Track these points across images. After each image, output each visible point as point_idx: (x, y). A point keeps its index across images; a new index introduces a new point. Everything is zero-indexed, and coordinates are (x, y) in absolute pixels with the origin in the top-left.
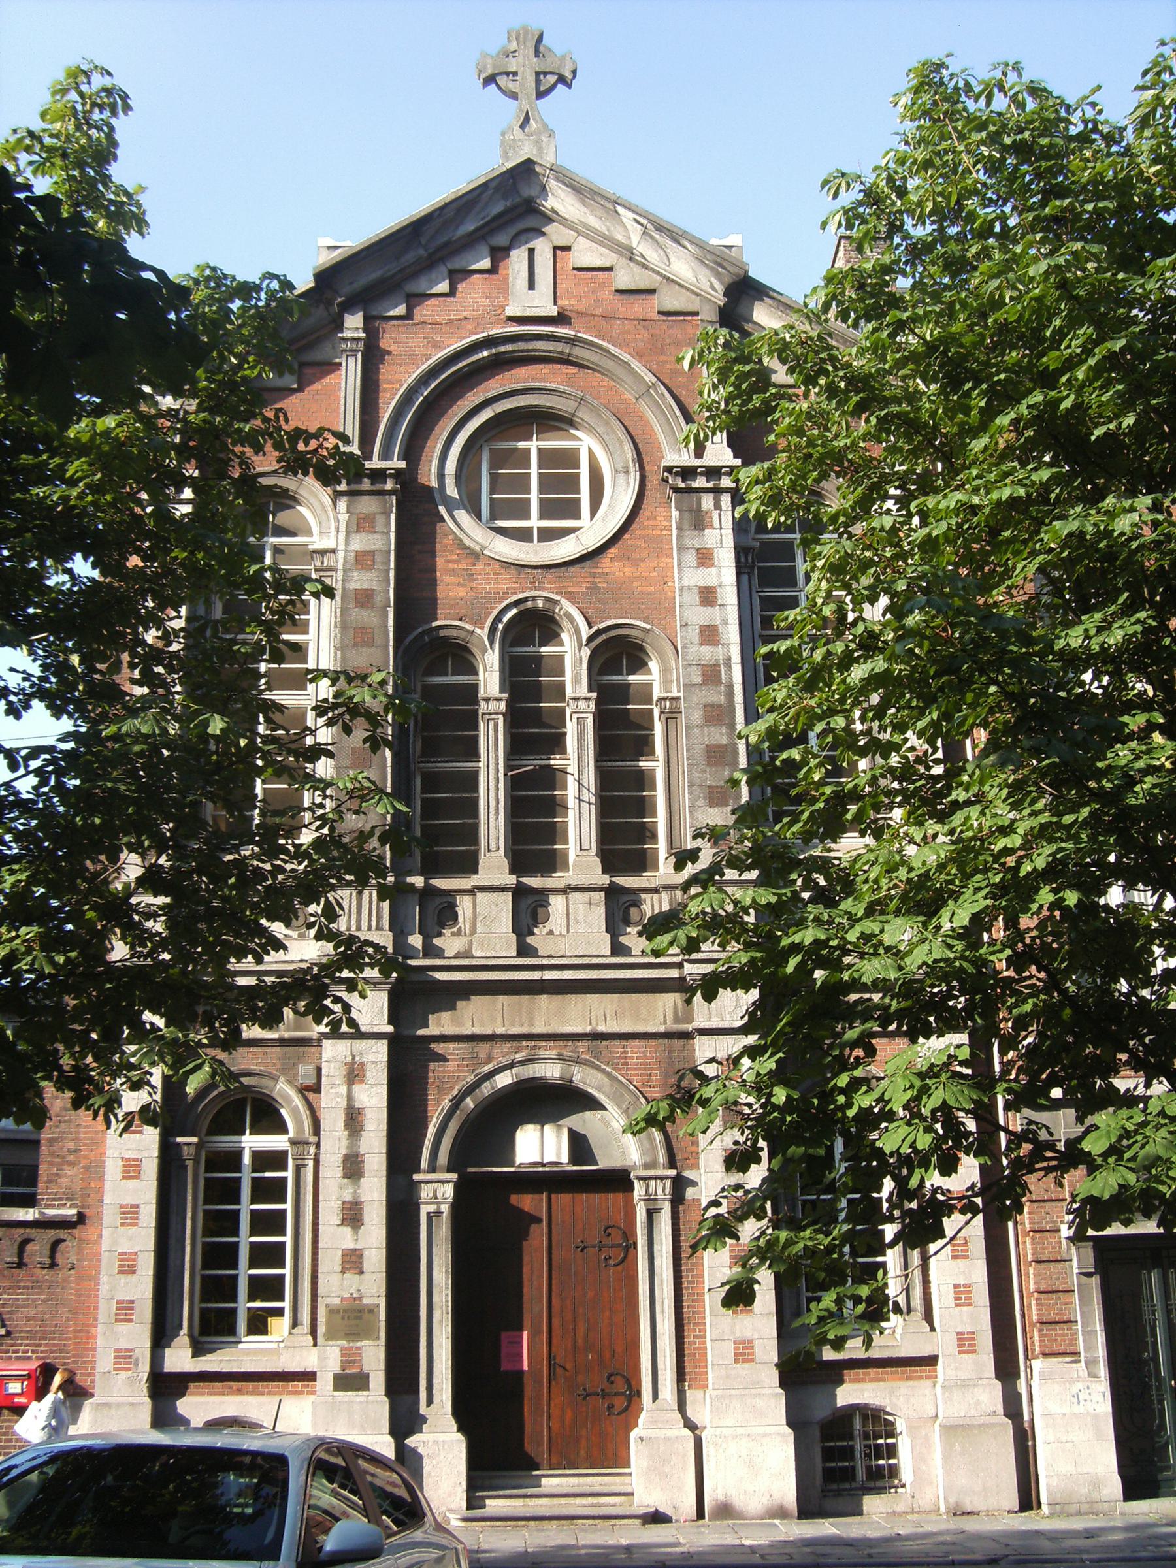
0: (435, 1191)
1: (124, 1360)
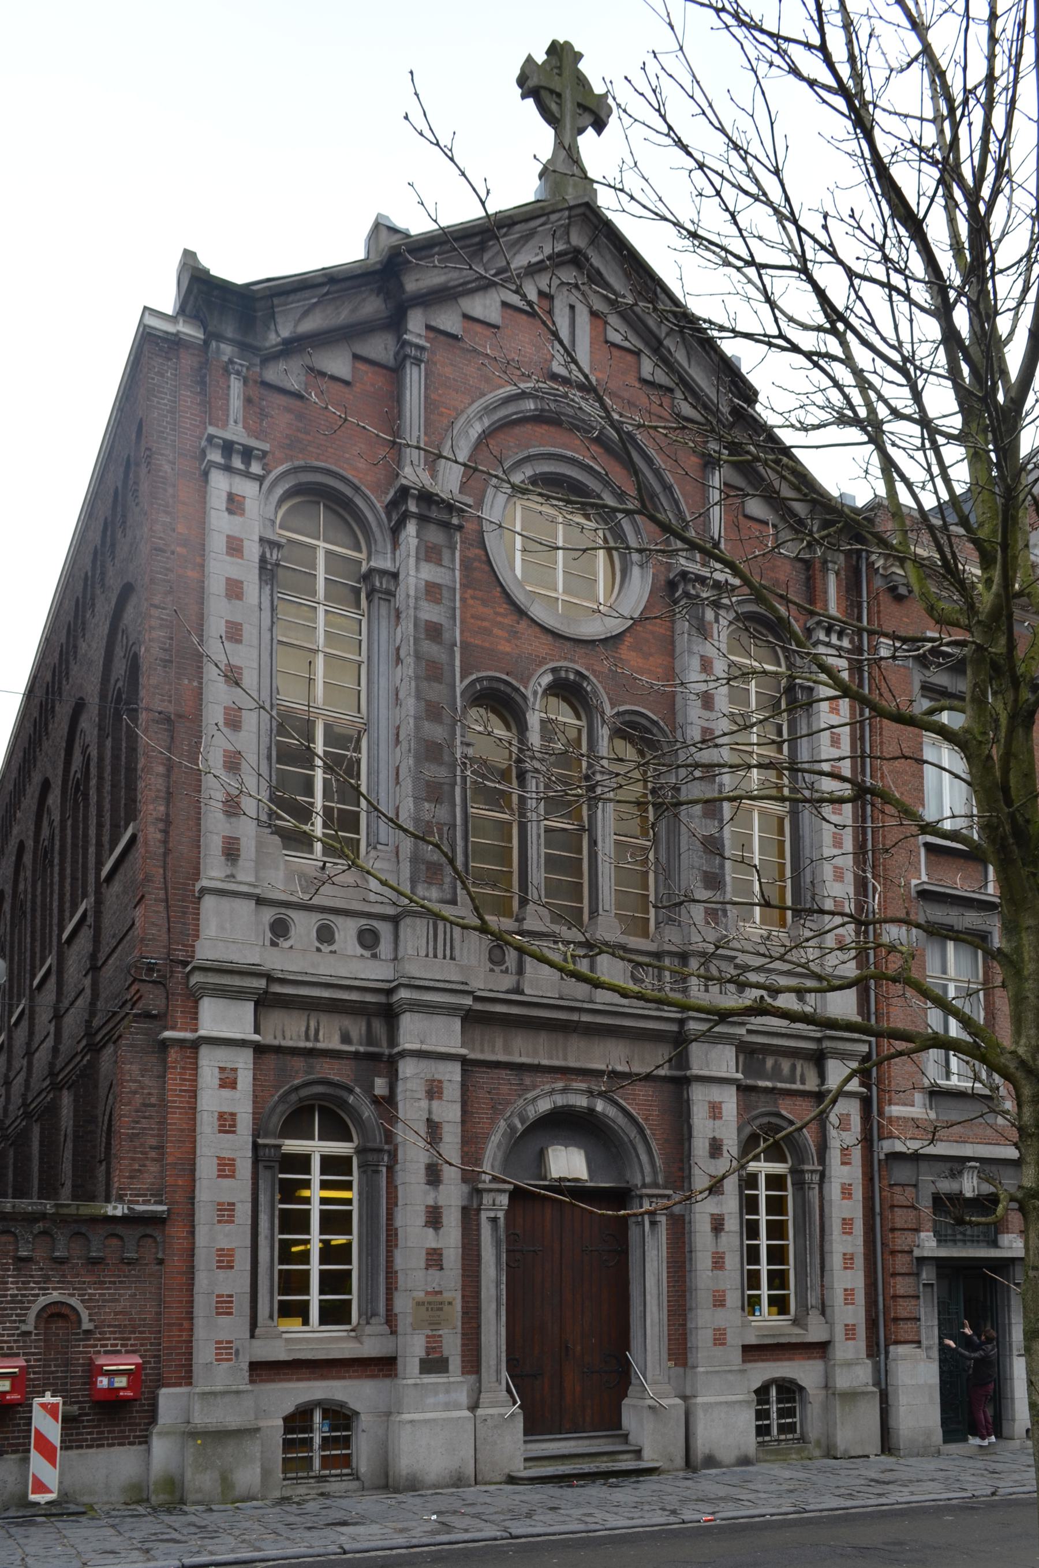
1: (225, 1350)
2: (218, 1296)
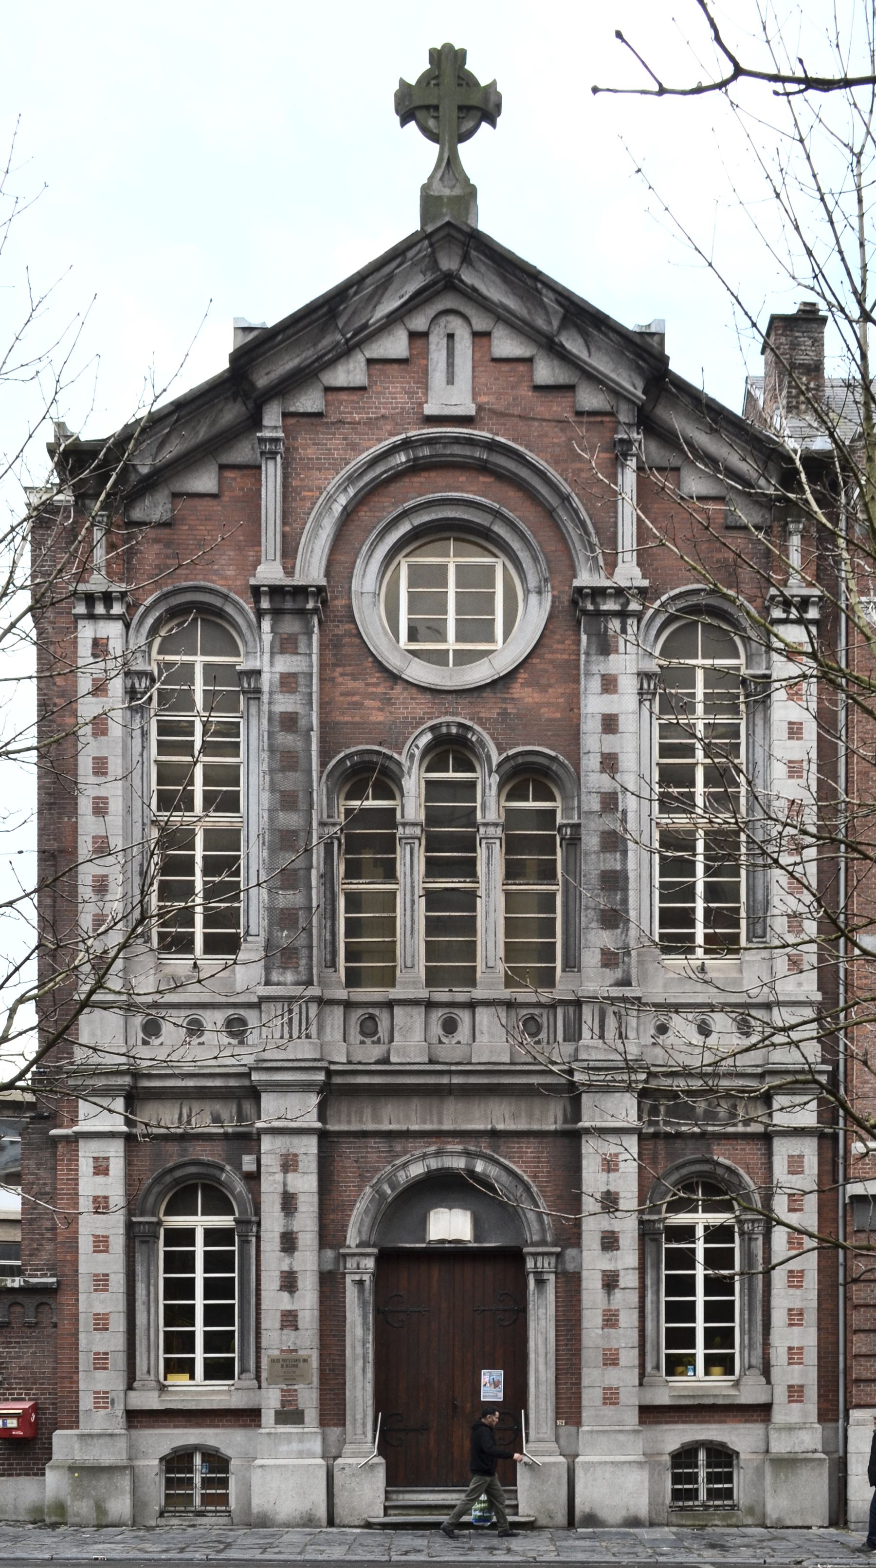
0: (358, 1265)
1: (102, 1399)
2: (95, 1354)
